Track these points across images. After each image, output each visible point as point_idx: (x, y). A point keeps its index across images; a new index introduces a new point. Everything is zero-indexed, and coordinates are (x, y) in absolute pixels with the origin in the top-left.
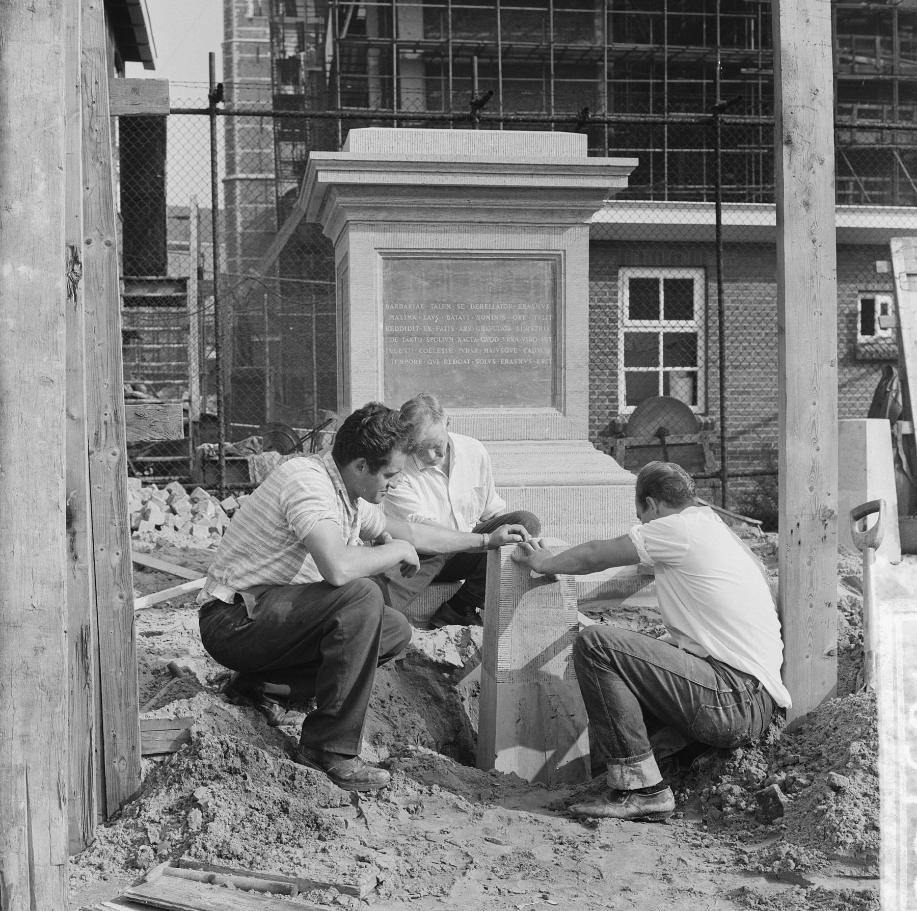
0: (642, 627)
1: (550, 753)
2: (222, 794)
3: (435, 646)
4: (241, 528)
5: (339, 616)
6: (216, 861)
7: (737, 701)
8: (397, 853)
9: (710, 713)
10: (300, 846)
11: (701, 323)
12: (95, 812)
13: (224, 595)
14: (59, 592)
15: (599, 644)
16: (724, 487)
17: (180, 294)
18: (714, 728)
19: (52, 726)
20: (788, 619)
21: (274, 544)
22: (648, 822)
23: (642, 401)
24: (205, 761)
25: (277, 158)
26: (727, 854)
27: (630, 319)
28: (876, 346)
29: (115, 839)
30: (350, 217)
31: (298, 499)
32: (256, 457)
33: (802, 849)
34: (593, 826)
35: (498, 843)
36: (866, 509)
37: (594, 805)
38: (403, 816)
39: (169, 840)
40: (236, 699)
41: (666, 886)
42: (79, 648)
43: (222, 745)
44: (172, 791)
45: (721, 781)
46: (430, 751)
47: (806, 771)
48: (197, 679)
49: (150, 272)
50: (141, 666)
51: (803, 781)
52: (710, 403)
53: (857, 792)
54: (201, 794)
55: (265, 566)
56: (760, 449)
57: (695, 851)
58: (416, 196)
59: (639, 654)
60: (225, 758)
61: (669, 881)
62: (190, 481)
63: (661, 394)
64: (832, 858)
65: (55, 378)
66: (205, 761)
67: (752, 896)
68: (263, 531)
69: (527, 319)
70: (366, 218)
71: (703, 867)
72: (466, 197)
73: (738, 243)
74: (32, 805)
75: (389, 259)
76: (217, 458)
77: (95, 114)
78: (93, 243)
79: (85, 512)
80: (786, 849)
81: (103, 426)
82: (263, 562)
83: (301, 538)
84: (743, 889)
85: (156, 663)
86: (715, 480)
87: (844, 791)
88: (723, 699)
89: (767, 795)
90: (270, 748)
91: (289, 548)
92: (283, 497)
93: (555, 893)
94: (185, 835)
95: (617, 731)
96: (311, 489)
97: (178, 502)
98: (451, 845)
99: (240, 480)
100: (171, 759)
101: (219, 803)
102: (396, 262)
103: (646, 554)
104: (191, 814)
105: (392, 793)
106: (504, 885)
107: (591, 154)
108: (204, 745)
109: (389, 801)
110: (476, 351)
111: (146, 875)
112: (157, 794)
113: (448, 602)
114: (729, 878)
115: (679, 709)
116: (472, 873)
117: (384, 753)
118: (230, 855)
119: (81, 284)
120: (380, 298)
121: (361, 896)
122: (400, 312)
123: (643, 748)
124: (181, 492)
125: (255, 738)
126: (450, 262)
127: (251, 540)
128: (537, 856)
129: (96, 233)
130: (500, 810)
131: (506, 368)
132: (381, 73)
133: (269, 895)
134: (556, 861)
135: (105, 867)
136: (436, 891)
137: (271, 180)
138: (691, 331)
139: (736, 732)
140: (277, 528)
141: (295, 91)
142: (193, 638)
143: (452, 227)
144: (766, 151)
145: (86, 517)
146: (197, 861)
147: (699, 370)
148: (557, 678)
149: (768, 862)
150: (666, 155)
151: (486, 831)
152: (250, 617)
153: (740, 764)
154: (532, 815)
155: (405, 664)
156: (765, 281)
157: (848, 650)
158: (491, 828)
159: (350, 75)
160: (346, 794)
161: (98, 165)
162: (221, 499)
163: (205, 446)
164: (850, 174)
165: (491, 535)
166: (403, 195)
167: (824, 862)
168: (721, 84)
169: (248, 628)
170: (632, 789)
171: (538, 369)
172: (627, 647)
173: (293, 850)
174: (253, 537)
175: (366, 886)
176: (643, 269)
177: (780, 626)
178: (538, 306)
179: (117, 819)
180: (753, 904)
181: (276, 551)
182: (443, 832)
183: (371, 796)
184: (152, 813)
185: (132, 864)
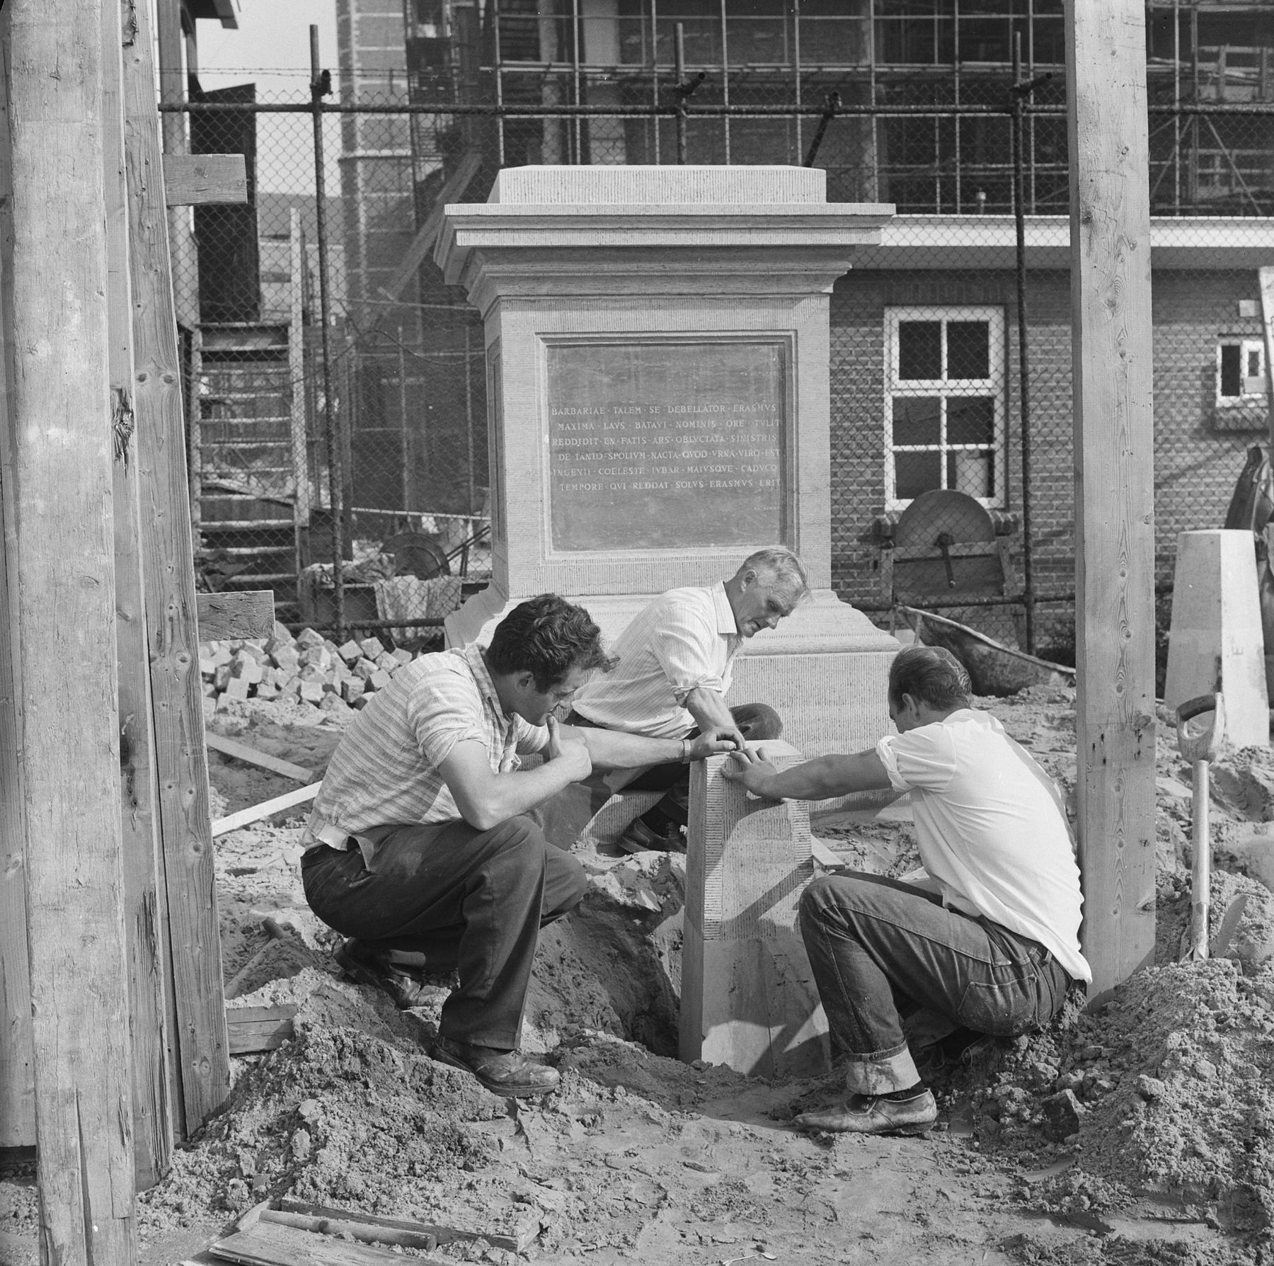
1: (776, 1030)
5: (487, 869)
6: (328, 1202)
7: (1017, 977)
8: (566, 1185)
9: (982, 993)
10: (438, 1180)
12: (171, 1133)
13: (333, 838)
15: (834, 903)
16: (1029, 617)
17: (278, 347)
18: (987, 1012)
19: (108, 1040)
20: (1089, 863)
21: (399, 771)
22: (901, 1136)
23: (921, 491)
24: (313, 1064)
26: (1002, 1184)
28: (1245, 412)
29: (197, 1170)
30: (501, 291)
31: (432, 712)
32: (386, 584)
33: (1100, 1182)
34: (827, 1144)
35: (700, 1169)
36: (1198, 706)
37: (829, 1114)
38: (577, 1130)
39: (268, 1172)
40: (353, 973)
41: (919, 1231)
42: (142, 921)
44: (271, 1103)
45: (999, 1081)
46: (613, 1039)
47: (1111, 1068)
48: (302, 942)
49: (236, 317)
50: (228, 923)
51: (1105, 1084)
53: (1174, 1101)
54: (309, 1109)
55: (387, 801)
58: (591, 261)
59: (886, 915)
62: (296, 618)
63: (945, 486)
64: (1138, 1194)
65: (101, 577)
66: (313, 1064)
67: (1031, 1247)
68: (385, 754)
70: (523, 292)
71: (970, 1203)
72: (660, 261)
74: (86, 1142)
75: (555, 347)
76: (332, 586)
78: (148, 380)
79: (146, 743)
80: (1080, 1180)
81: (169, 624)
82: (387, 795)
83: (435, 764)
84: (1020, 1236)
85: (247, 918)
86: (1018, 606)
88: (999, 974)
90: (399, 1040)
91: (420, 776)
92: (412, 708)
93: (774, 1243)
95: (858, 1019)
96: (449, 699)
98: (638, 1174)
99: (364, 617)
100: (268, 1060)
101: (332, 1122)
102: (565, 351)
104: (296, 1137)
105: (562, 1099)
106: (707, 1231)
107: (830, 199)
108: (312, 1042)
109: (557, 1112)
110: (676, 470)
111: (238, 1219)
112: (251, 1108)
113: (643, 817)
114: (1003, 1219)
116: (665, 1214)
117: (553, 1039)
118: (347, 1195)
119: (134, 439)
120: (544, 401)
121: (519, 1250)
122: (572, 419)
123: (894, 1039)
124: (283, 635)
125: (376, 1029)
126: (639, 349)
127: (369, 765)
128: (752, 1189)
129: (152, 365)
130: (705, 1121)
131: (717, 493)
132: (557, 12)
133: (398, 1249)
134: (776, 1196)
135: (185, 1208)
136: (617, 1240)
137: (406, 157)
140: (404, 750)
141: (437, 32)
143: (641, 302)
145: (147, 751)
146: (304, 1202)
148: (786, 929)
149: (1055, 1198)
151: (686, 1151)
152: (368, 869)
153: (1024, 1057)
154: (748, 1126)
155: (582, 909)
157: (1170, 899)
158: (692, 1147)
159: (513, 16)
160: (501, 1101)
161: (152, 274)
162: (338, 643)
163: (316, 566)
164: (1217, 147)
167: (1127, 1199)
168: (1035, 20)
169: (366, 884)
170: (880, 1093)
171: (761, 493)
172: (870, 907)
173: (430, 1186)
174: (371, 760)
175: (525, 1235)
177: (1079, 872)
178: (761, 407)
179: (200, 1139)
180: (1032, 1259)
181: (402, 779)
182: (628, 1154)
183: (533, 1103)
184: (245, 1134)
185: (220, 1204)
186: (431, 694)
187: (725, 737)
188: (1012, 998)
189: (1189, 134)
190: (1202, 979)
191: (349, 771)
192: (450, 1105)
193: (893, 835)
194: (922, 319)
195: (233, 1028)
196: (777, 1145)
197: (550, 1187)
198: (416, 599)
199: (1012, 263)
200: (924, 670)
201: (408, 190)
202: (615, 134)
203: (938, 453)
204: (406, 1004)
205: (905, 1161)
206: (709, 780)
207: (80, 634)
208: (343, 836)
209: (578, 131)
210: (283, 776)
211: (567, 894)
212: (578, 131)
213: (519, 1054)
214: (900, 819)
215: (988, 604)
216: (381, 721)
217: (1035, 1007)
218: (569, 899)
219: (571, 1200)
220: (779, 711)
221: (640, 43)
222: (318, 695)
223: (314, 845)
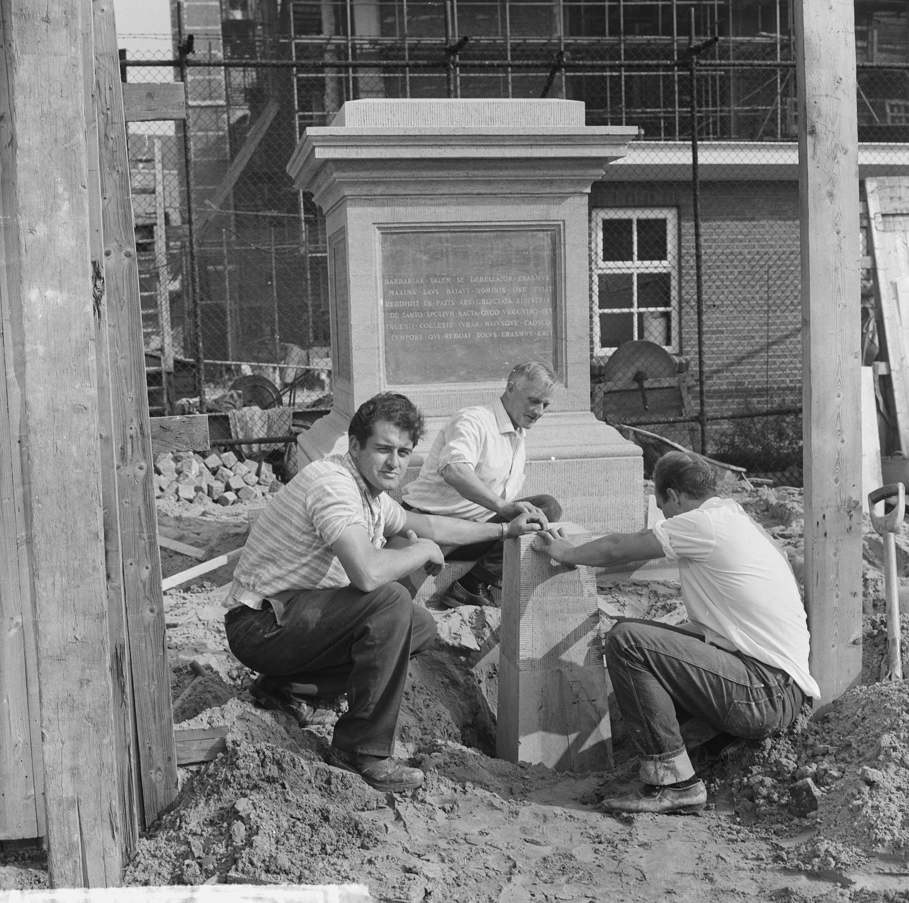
0: (652, 602)
1: (573, 737)
2: (262, 804)
3: (450, 629)
4: (266, 532)
8: (439, 859)
9: (743, 708)
11: (674, 263)
13: (251, 601)
14: (101, 622)
15: (633, 643)
16: (703, 431)
18: (748, 723)
19: (101, 758)
20: (815, 610)
21: (301, 549)
22: (681, 814)
25: (228, 85)
27: (604, 260)
29: (158, 853)
31: (325, 504)
34: (629, 822)
35: (537, 843)
37: (628, 799)
38: (440, 816)
39: (213, 854)
41: (708, 887)
43: (259, 753)
44: (212, 802)
45: (751, 772)
51: (835, 773)
52: (684, 343)
53: (890, 785)
54: (242, 805)
56: (733, 387)
57: (732, 846)
59: (672, 652)
60: (263, 766)
61: (711, 880)
63: (636, 338)
64: (871, 855)
65: (89, 405)
66: (243, 771)
67: (796, 897)
68: (289, 537)
69: (528, 291)
71: (742, 864)
72: (465, 170)
73: (711, 182)
75: (387, 233)
77: (110, 121)
81: (129, 440)
82: (291, 567)
83: (329, 543)
84: (787, 889)
85: (177, 661)
86: (694, 424)
87: (878, 785)
88: (755, 694)
89: (801, 789)
90: (303, 751)
91: (316, 553)
92: (309, 502)
93: (601, 898)
94: (230, 848)
95: (651, 729)
96: (339, 494)
97: (162, 462)
98: (492, 848)
99: (223, 436)
100: (207, 769)
101: (261, 814)
102: (395, 236)
103: (672, 550)
104: (234, 827)
108: (241, 754)
109: (425, 802)
112: (197, 805)
113: (459, 581)
114: (769, 876)
115: (711, 705)
116: (517, 879)
118: (277, 871)
119: (104, 300)
120: (379, 274)
123: (677, 744)
126: (449, 235)
127: (277, 545)
128: (578, 857)
130: (535, 807)
131: (508, 341)
137: (222, 106)
138: (665, 271)
139: (768, 726)
140: (304, 533)
141: (243, 15)
142: (209, 630)
144: (722, 73)
146: (244, 876)
147: (673, 309)
149: (807, 859)
150: (623, 78)
151: (524, 830)
152: (279, 623)
153: (769, 754)
154: (566, 810)
156: (737, 220)
160: (381, 795)
161: (115, 174)
165: (509, 524)
166: (404, 169)
169: (277, 635)
172: (660, 646)
173: (339, 862)
174: (279, 542)
176: (616, 210)
178: (538, 278)
179: (156, 830)
183: (406, 796)
184: (193, 826)
186: (324, 490)
187: (533, 521)
188: (765, 712)
189: (787, 86)
190: (901, 695)
191: (262, 550)
192: (345, 799)
193: (645, 591)
194: (616, 217)
195: (179, 745)
196: (591, 823)
197: (428, 860)
198: (260, 423)
199: (689, 176)
200: (682, 470)
201: (223, 130)
202: (377, 88)
203: (632, 314)
204: (303, 724)
205: (689, 834)
206: (523, 553)
207: (74, 449)
208: (259, 599)
209: (351, 86)
210: (182, 555)
211: (425, 638)
212: (351, 86)
213: (393, 759)
214: (649, 579)
215: (674, 422)
216: (285, 512)
217: (779, 720)
218: (426, 642)
219: (446, 870)
220: (561, 502)
221: (395, 22)
222: (191, 494)
223: (236, 606)
